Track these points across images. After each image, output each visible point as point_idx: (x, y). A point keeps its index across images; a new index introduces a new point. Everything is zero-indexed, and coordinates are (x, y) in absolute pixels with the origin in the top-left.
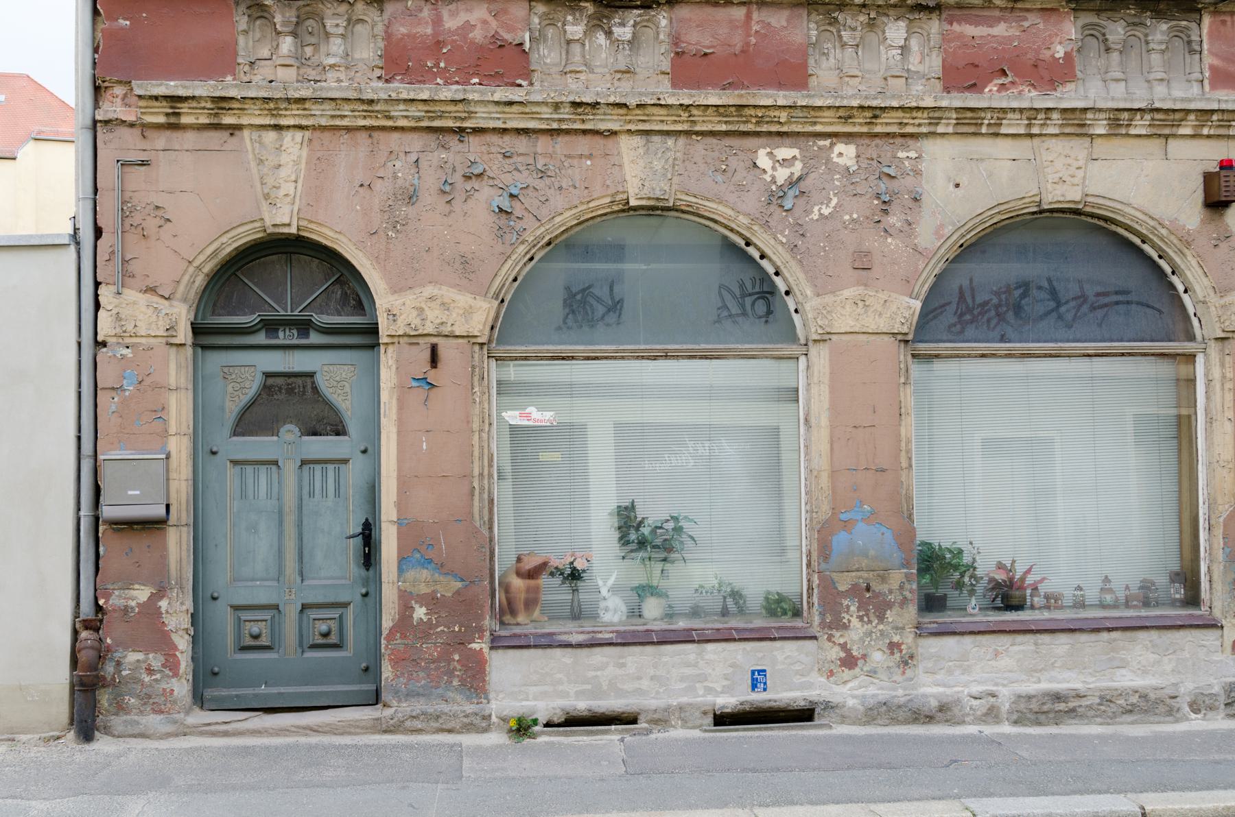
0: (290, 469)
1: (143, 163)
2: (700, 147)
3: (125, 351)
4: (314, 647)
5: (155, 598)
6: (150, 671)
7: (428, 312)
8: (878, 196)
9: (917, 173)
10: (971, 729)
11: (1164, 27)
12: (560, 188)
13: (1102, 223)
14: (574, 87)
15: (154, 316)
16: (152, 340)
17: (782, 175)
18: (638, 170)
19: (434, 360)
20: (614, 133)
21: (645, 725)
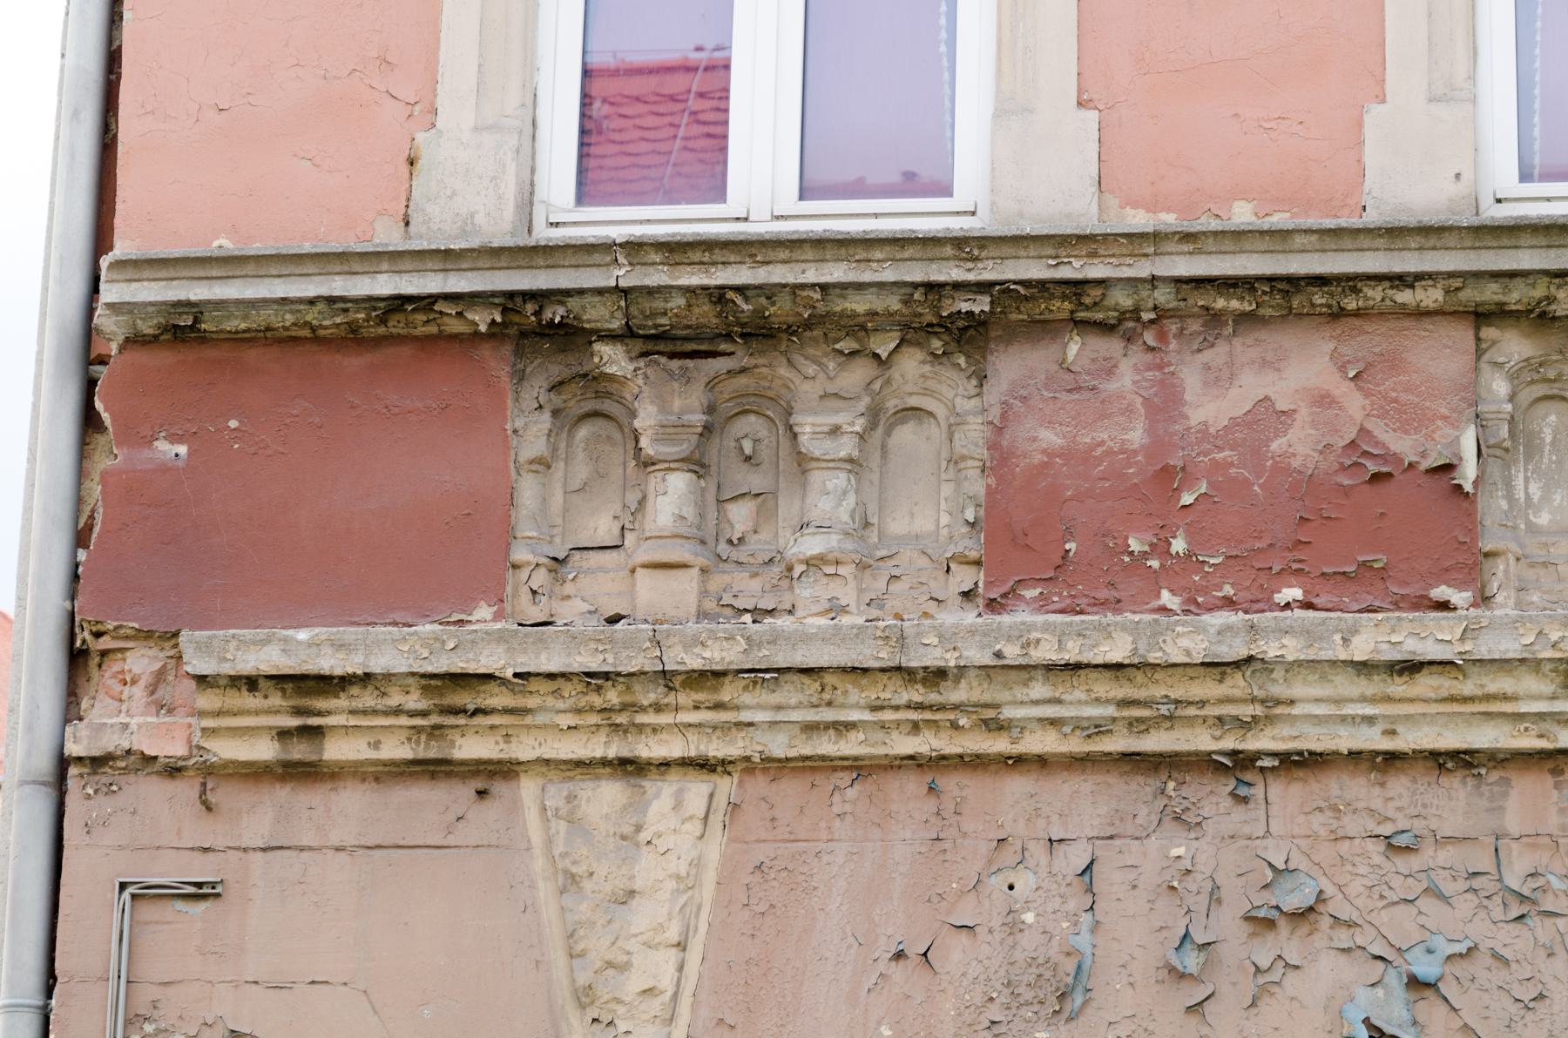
1: (202, 892)
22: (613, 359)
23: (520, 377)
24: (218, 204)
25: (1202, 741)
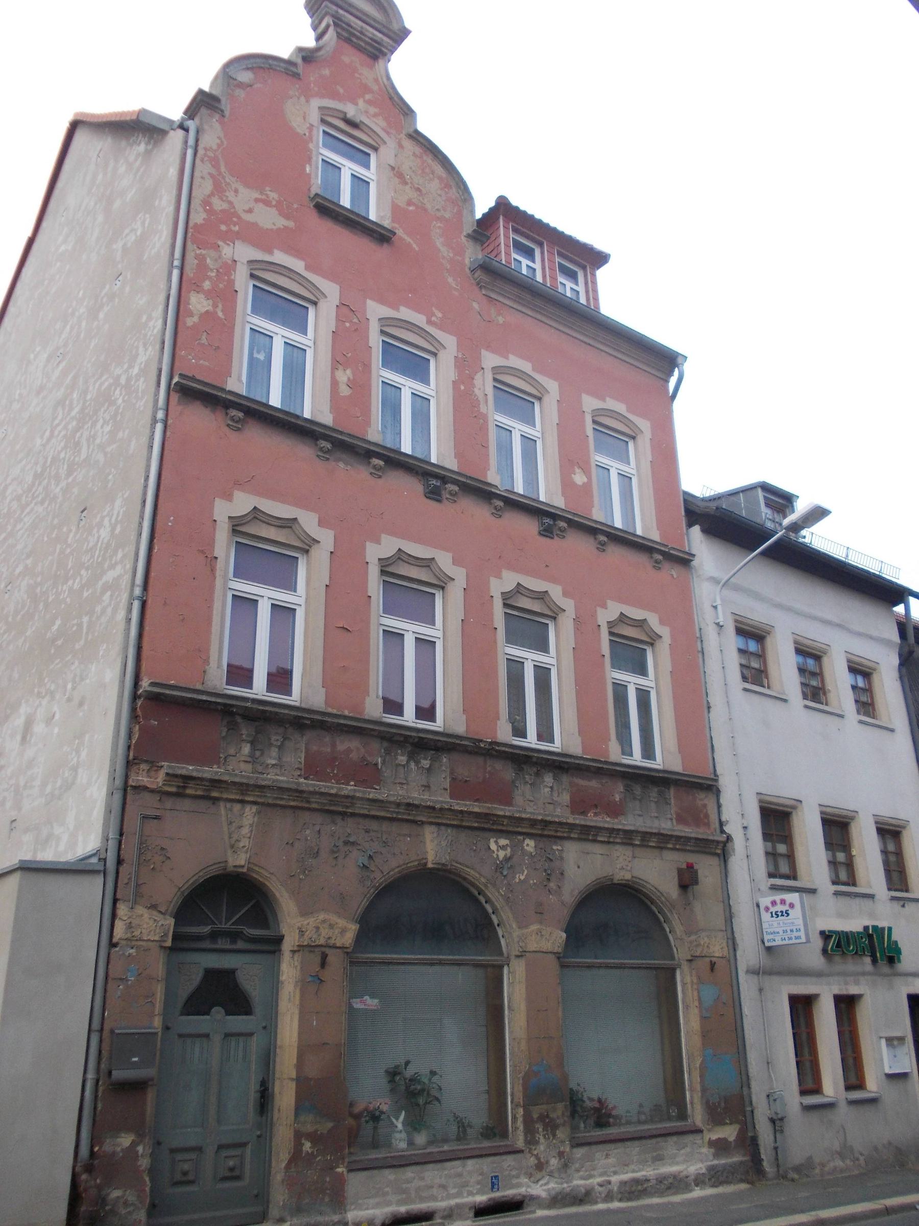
0: (217, 1039)
1: (157, 818)
2: (463, 836)
3: (131, 951)
4: (225, 1179)
5: (134, 1144)
6: (126, 1204)
7: (322, 930)
8: (545, 871)
9: (562, 858)
10: (601, 1206)
11: (656, 790)
12: (394, 854)
13: (634, 892)
14: (400, 792)
15: (151, 925)
16: (150, 943)
17: (502, 854)
18: (433, 847)
19: (323, 964)
20: (423, 823)
21: (439, 1221)
22: (239, 719)
23: (222, 720)
24: (164, 673)
25: (340, 809)
